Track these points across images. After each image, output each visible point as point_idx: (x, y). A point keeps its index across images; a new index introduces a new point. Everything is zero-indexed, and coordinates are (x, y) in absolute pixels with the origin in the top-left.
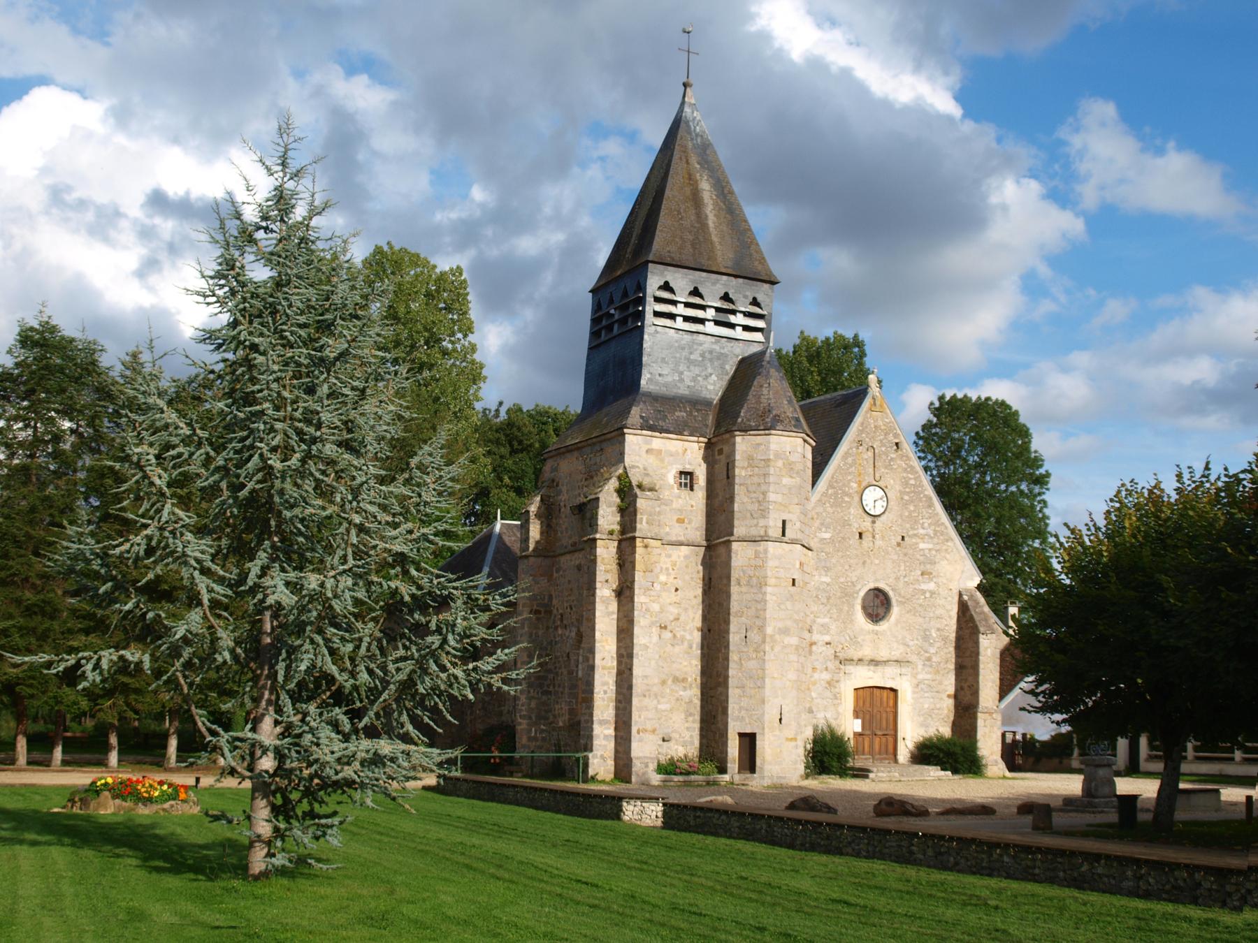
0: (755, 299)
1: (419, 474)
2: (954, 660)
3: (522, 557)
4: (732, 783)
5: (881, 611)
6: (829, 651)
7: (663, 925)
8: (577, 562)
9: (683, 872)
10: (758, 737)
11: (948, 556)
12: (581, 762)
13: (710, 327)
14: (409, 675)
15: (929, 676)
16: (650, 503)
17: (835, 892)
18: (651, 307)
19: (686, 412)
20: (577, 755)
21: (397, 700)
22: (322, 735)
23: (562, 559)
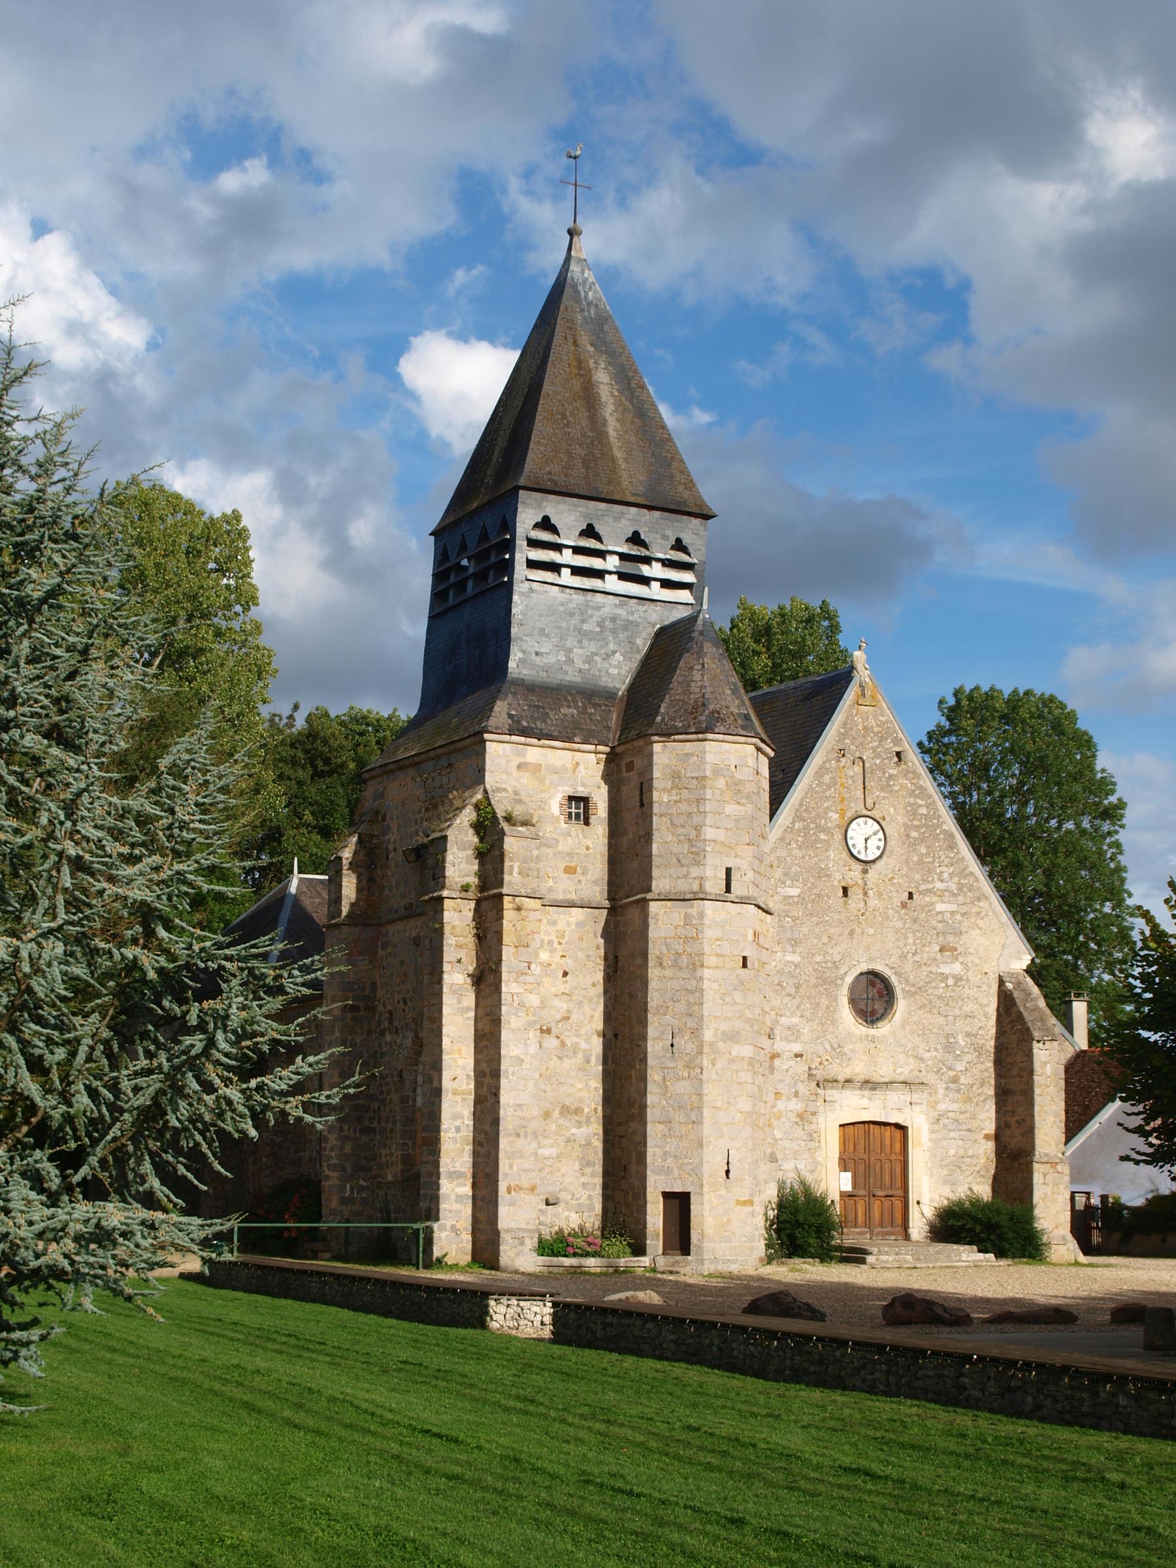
0: (678, 541)
1: (171, 782)
2: (993, 1082)
3: (329, 927)
4: (654, 1270)
5: (879, 1006)
6: (801, 1068)
7: (572, 1513)
8: (414, 934)
9: (593, 1417)
10: (693, 1199)
11: (980, 923)
12: (422, 1236)
13: (612, 583)
14: (155, 1098)
15: (955, 1107)
16: (525, 843)
18: (523, 553)
19: (577, 707)
20: (415, 1226)
22: (13, 1195)
23: (392, 928)
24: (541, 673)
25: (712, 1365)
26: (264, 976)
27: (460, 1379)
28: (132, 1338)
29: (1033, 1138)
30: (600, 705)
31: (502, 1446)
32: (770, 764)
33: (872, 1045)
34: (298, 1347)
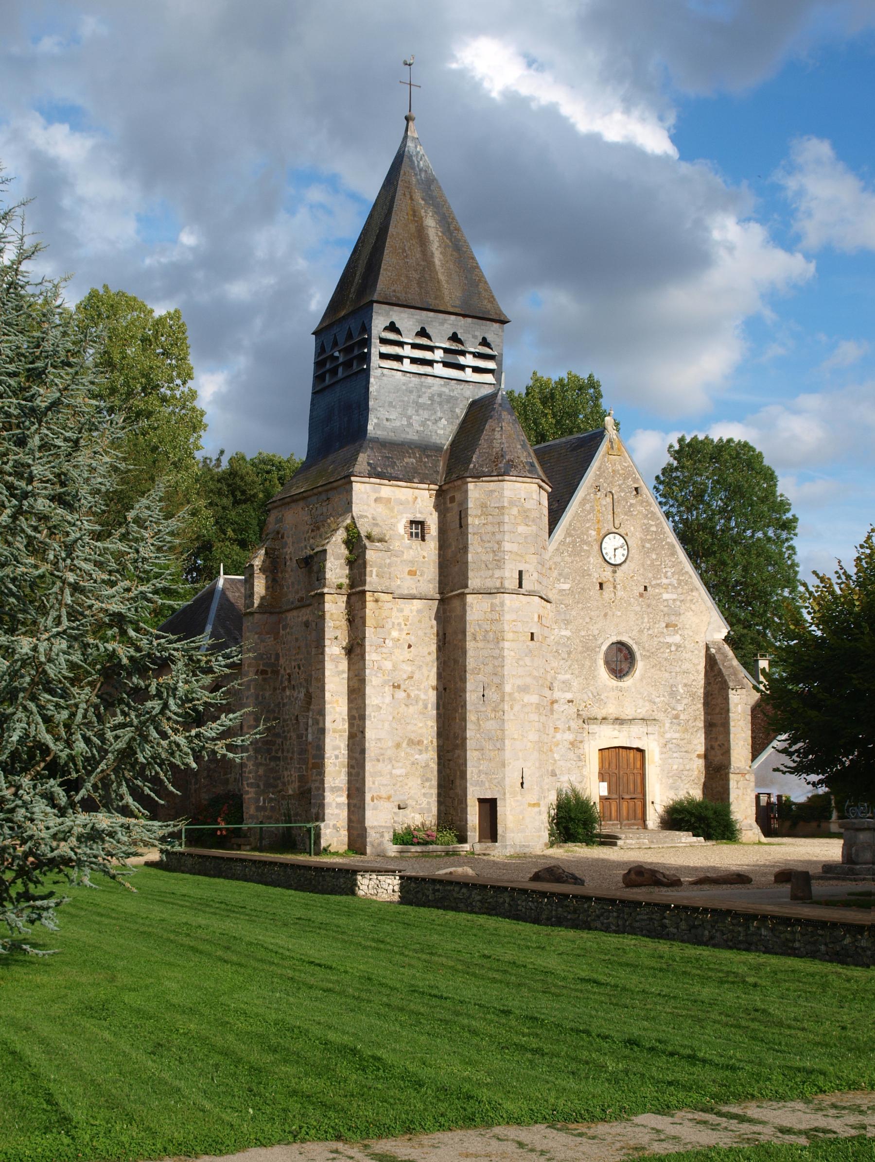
0: (484, 339)
1: (136, 528)
2: (703, 718)
4: (473, 853)
5: (625, 666)
6: (572, 710)
7: (402, 1010)
8: (305, 619)
9: (422, 951)
11: (693, 607)
12: (313, 832)
13: (439, 369)
14: (129, 744)
15: (677, 735)
16: (381, 554)
17: (583, 970)
18: (377, 348)
19: (415, 458)
20: (308, 825)
21: (116, 770)
22: (36, 810)
23: (289, 615)
24: (390, 434)
25: (505, 916)
26: (199, 661)
27: (335, 929)
28: (113, 907)
29: (730, 757)
30: (431, 456)
31: (361, 970)
32: (548, 496)
33: (620, 694)
34: (227, 910)
